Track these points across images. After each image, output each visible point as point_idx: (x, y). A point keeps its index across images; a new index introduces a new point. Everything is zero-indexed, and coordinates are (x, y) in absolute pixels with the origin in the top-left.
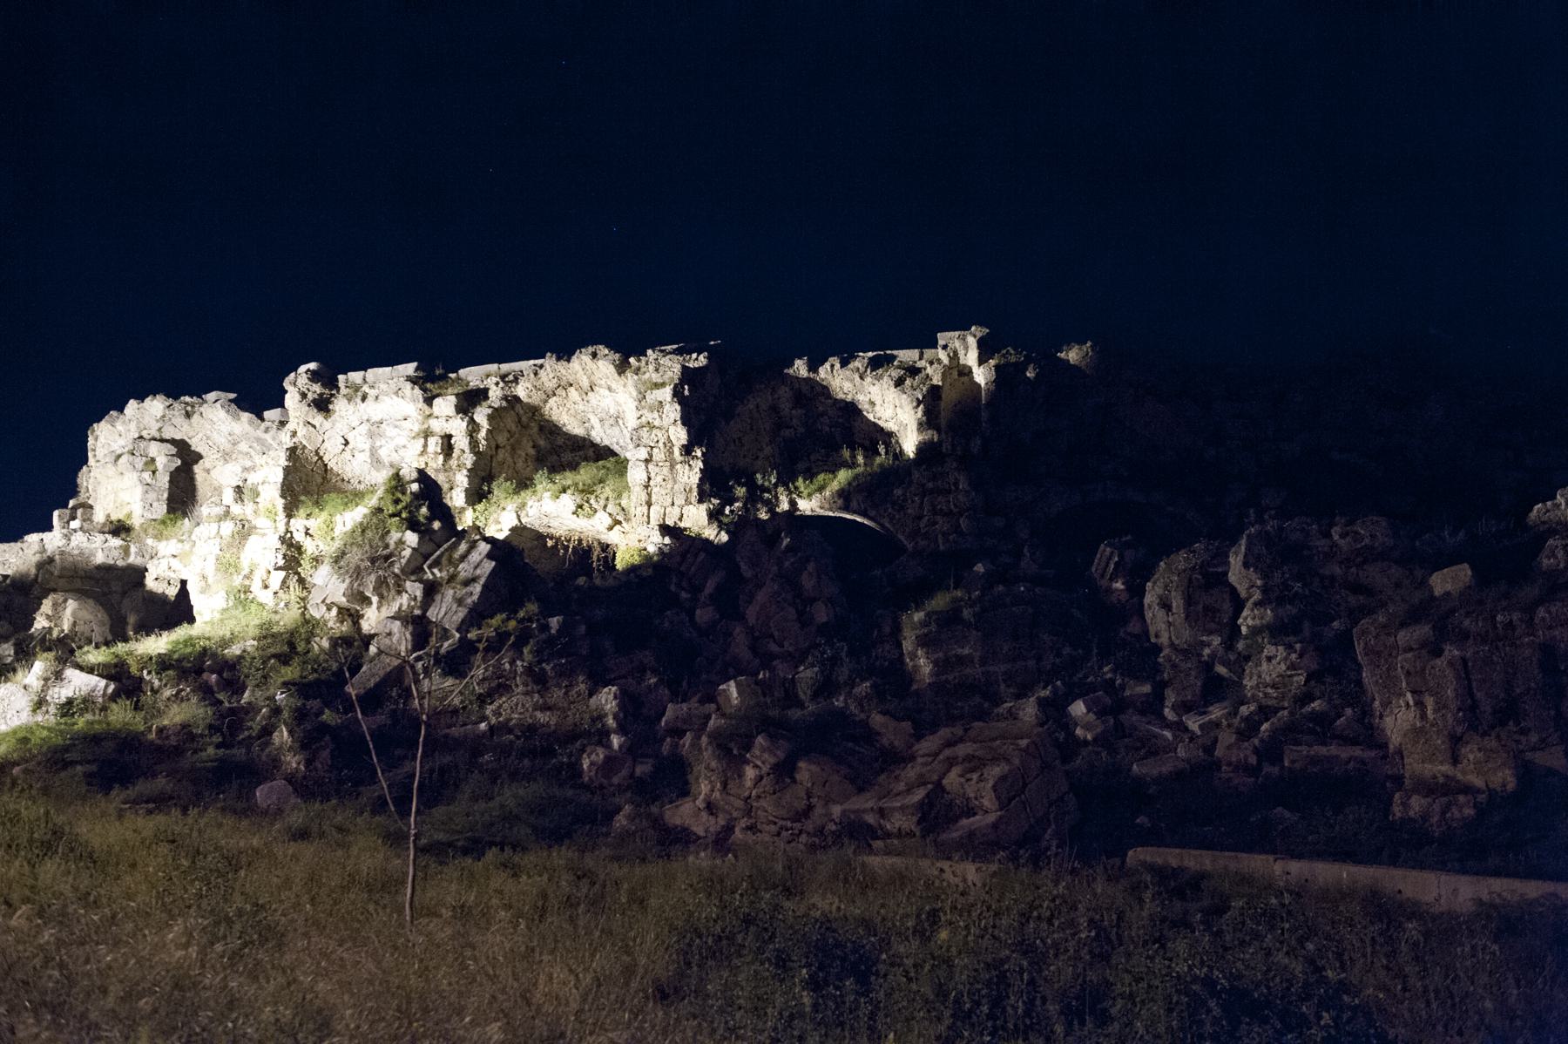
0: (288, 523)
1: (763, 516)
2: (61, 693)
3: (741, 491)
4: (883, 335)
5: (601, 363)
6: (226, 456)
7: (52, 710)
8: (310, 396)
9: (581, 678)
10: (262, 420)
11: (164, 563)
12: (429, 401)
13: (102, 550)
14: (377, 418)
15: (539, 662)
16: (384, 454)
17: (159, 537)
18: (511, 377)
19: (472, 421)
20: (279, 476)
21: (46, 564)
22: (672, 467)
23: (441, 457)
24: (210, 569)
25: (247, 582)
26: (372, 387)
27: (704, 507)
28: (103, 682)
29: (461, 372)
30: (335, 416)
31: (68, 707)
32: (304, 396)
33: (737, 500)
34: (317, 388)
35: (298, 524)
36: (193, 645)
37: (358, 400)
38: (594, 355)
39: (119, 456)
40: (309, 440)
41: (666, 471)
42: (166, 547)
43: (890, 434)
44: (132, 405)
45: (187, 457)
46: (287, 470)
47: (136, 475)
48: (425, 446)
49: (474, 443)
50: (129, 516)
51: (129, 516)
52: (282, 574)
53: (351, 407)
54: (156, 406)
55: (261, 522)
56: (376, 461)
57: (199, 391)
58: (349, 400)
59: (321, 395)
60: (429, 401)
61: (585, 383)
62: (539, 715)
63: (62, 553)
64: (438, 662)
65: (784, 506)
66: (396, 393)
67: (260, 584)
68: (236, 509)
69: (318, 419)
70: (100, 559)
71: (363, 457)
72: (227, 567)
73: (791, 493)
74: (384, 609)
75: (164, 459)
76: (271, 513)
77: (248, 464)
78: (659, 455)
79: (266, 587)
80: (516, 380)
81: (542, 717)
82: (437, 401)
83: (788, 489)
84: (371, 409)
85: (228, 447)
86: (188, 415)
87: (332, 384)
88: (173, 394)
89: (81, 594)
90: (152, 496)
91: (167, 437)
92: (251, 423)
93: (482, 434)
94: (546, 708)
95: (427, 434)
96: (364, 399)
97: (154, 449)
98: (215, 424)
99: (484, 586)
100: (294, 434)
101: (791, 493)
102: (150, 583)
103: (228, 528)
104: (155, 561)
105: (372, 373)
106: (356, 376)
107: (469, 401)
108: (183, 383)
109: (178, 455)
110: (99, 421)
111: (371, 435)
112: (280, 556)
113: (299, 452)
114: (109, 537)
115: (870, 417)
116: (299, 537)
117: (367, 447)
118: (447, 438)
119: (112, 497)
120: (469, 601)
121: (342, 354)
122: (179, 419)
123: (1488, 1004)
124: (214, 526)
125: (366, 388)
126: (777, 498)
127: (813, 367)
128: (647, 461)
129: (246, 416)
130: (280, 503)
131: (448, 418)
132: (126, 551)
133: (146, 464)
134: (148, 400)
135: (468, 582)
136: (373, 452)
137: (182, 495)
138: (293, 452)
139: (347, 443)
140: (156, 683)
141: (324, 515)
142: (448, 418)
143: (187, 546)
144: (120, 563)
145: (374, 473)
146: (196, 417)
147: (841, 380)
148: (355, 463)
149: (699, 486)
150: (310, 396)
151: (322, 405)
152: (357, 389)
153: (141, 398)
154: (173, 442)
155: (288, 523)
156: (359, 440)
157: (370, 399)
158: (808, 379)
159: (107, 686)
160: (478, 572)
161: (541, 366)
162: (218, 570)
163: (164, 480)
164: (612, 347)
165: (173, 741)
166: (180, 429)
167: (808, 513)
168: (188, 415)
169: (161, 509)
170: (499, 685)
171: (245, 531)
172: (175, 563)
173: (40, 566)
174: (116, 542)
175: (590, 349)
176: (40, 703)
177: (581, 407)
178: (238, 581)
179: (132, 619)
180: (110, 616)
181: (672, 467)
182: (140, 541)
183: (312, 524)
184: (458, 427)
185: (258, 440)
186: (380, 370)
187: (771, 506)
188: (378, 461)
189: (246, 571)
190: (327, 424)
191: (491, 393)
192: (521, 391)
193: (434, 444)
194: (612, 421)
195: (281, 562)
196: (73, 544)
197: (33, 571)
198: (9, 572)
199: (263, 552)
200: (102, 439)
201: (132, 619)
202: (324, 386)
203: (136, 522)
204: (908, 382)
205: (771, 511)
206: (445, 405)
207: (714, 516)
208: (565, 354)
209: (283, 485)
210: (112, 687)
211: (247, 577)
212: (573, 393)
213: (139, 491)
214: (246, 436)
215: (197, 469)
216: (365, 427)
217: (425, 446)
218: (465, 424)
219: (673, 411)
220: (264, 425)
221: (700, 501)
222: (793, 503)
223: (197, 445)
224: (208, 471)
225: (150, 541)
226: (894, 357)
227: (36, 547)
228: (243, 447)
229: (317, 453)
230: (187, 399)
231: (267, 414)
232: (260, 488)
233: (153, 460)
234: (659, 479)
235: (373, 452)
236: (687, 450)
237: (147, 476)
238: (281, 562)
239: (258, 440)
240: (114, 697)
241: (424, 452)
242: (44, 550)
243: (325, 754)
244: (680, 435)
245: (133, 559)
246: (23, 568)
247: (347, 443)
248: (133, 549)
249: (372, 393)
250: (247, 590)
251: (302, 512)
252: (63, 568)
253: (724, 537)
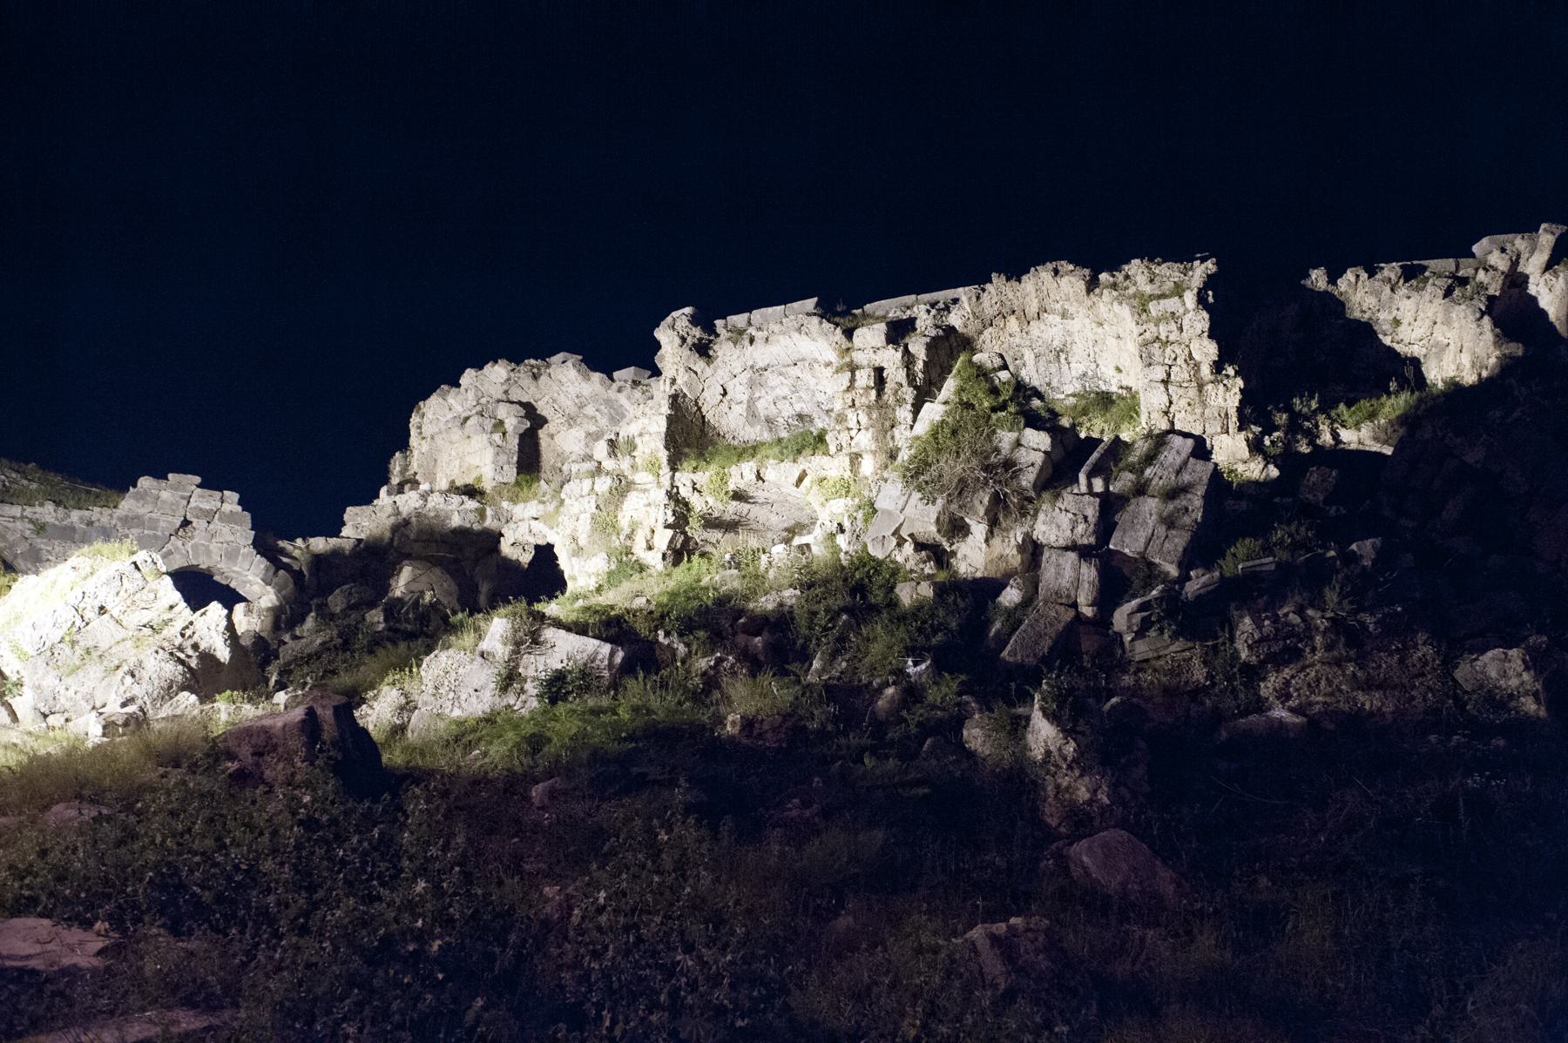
0: (673, 477)
1: (1304, 448)
2: (537, 666)
3: (1282, 418)
4: (1422, 239)
5: (1064, 281)
6: (571, 421)
7: (531, 689)
8: (690, 340)
9: (1421, 637)
10: (613, 380)
11: (523, 528)
12: (849, 333)
13: (459, 514)
14: (761, 364)
15: (1356, 612)
16: (762, 406)
17: (514, 500)
18: (941, 305)
19: (906, 351)
20: (662, 425)
21: (401, 526)
22: (1200, 387)
23: (873, 393)
24: (584, 528)
25: (628, 543)
26: (759, 329)
27: (1242, 435)
28: (606, 648)
29: (868, 307)
30: (718, 362)
31: (556, 687)
32: (684, 340)
33: (1277, 428)
34: (697, 332)
35: (684, 479)
36: (697, 597)
37: (747, 342)
38: (1056, 272)
39: (467, 419)
40: (690, 386)
41: (1193, 392)
42: (525, 510)
43: (1415, 362)
44: (468, 377)
45: (534, 419)
46: (669, 418)
47: (485, 437)
48: (853, 380)
49: (911, 378)
50: (479, 479)
51: (479, 479)
52: (670, 532)
53: (737, 352)
54: (498, 372)
55: (643, 477)
56: (752, 415)
57: (544, 353)
58: (735, 344)
59: (700, 339)
60: (849, 333)
61: (1033, 308)
62: (1361, 697)
63: (418, 515)
64: (1170, 614)
65: (1326, 438)
66: (799, 330)
67: (644, 545)
68: (609, 464)
69: (700, 365)
70: (456, 521)
71: (739, 410)
72: (604, 525)
73: (1333, 421)
74: (996, 541)
75: (513, 421)
76: (653, 467)
77: (593, 429)
78: (1180, 373)
79: (650, 548)
80: (947, 309)
81: (1368, 701)
82: (857, 332)
83: (1329, 417)
84: (759, 354)
85: (573, 410)
86: (535, 377)
87: (710, 329)
88: (516, 359)
89: (432, 561)
90: (503, 458)
91: (514, 398)
92: (602, 383)
93: (920, 365)
94: (1368, 686)
95: (853, 368)
96: (752, 341)
97: (503, 411)
98: (565, 384)
99: (1206, 497)
100: (674, 381)
101: (1333, 421)
102: (506, 548)
103: (604, 484)
104: (512, 525)
105: (757, 315)
106: (738, 320)
107: (899, 331)
108: (527, 347)
109: (527, 416)
110: (426, 397)
111: (752, 385)
112: (670, 513)
113: (680, 400)
114: (465, 498)
115: (1387, 341)
116: (685, 492)
117: (745, 398)
118: (879, 371)
119: (457, 463)
120: (1187, 520)
121: (727, 292)
122: (526, 381)
123: (1441, 883)
124: (587, 483)
125: (752, 331)
126: (1317, 426)
127: (1333, 280)
128: (1166, 382)
129: (597, 377)
130: (663, 455)
131: (876, 350)
132: (482, 514)
133: (495, 426)
134: (488, 368)
135: (1172, 494)
136: (751, 403)
137: (529, 460)
138: (675, 400)
139: (725, 393)
140: (681, 649)
141: (713, 469)
142: (876, 350)
143: (551, 507)
144: (476, 527)
145: (748, 428)
146: (543, 378)
147: (1361, 294)
148: (731, 416)
149: (1239, 410)
150: (690, 340)
151: (703, 350)
152: (741, 332)
153: (479, 366)
154: (520, 403)
155: (673, 477)
156: (738, 391)
157: (759, 342)
158: (1326, 292)
159: (612, 654)
160: (1186, 477)
161: (956, 301)
162: (594, 530)
163: (514, 443)
164: (1078, 262)
165: (771, 741)
166: (527, 390)
167: (1353, 446)
168: (535, 377)
169: (510, 474)
170: (1286, 649)
171: (622, 487)
172: (535, 525)
173: (395, 529)
174: (472, 504)
175: (1050, 266)
176: (510, 679)
177: (1017, 340)
178: (616, 543)
179: (485, 588)
180: (459, 585)
181: (1200, 387)
182: (494, 504)
183: (702, 478)
184: (891, 359)
185: (608, 402)
186: (770, 310)
187: (1312, 436)
188: (754, 416)
189: (627, 531)
190: (709, 371)
191: (918, 324)
192: (955, 319)
193: (864, 378)
194: (1052, 356)
195: (671, 520)
196: (430, 505)
197: (388, 535)
198: (363, 536)
199: (646, 513)
200: (429, 415)
201: (485, 588)
202: (704, 329)
203: (487, 486)
204: (1457, 292)
205: (1312, 443)
206: (870, 337)
207: (1256, 447)
208: (1016, 272)
209: (667, 434)
210: (619, 657)
211: (629, 537)
212: (1013, 323)
213: (489, 453)
214: (594, 398)
215: (542, 433)
216: (747, 374)
217: (853, 380)
218: (899, 355)
219: (1198, 321)
220: (615, 386)
221: (1240, 429)
222: (1335, 436)
223: (543, 409)
224: (552, 436)
225: (505, 504)
226: (1425, 268)
227: (389, 510)
228: (590, 410)
229: (697, 404)
230: (533, 361)
231: (616, 374)
232: (638, 441)
233: (501, 423)
234: (1183, 402)
235: (751, 403)
236: (1218, 367)
237: (497, 437)
238: (671, 520)
239: (608, 402)
240: (627, 669)
241: (851, 388)
242: (397, 513)
243: (1140, 772)
244: (1207, 351)
245: (489, 523)
246: (377, 532)
247: (725, 393)
248: (489, 512)
249: (759, 335)
250: (629, 552)
251: (687, 465)
252: (421, 532)
253: (1274, 472)
